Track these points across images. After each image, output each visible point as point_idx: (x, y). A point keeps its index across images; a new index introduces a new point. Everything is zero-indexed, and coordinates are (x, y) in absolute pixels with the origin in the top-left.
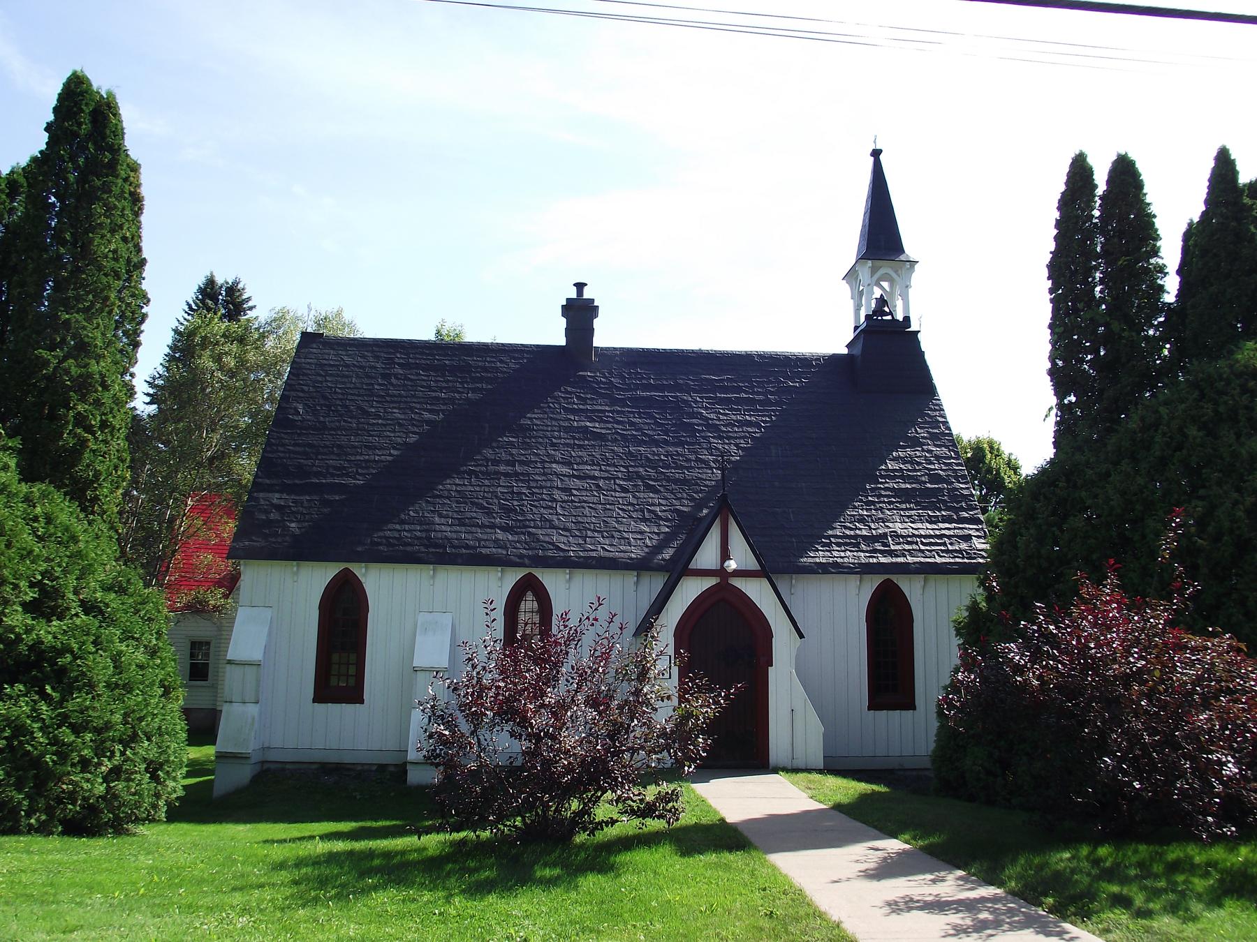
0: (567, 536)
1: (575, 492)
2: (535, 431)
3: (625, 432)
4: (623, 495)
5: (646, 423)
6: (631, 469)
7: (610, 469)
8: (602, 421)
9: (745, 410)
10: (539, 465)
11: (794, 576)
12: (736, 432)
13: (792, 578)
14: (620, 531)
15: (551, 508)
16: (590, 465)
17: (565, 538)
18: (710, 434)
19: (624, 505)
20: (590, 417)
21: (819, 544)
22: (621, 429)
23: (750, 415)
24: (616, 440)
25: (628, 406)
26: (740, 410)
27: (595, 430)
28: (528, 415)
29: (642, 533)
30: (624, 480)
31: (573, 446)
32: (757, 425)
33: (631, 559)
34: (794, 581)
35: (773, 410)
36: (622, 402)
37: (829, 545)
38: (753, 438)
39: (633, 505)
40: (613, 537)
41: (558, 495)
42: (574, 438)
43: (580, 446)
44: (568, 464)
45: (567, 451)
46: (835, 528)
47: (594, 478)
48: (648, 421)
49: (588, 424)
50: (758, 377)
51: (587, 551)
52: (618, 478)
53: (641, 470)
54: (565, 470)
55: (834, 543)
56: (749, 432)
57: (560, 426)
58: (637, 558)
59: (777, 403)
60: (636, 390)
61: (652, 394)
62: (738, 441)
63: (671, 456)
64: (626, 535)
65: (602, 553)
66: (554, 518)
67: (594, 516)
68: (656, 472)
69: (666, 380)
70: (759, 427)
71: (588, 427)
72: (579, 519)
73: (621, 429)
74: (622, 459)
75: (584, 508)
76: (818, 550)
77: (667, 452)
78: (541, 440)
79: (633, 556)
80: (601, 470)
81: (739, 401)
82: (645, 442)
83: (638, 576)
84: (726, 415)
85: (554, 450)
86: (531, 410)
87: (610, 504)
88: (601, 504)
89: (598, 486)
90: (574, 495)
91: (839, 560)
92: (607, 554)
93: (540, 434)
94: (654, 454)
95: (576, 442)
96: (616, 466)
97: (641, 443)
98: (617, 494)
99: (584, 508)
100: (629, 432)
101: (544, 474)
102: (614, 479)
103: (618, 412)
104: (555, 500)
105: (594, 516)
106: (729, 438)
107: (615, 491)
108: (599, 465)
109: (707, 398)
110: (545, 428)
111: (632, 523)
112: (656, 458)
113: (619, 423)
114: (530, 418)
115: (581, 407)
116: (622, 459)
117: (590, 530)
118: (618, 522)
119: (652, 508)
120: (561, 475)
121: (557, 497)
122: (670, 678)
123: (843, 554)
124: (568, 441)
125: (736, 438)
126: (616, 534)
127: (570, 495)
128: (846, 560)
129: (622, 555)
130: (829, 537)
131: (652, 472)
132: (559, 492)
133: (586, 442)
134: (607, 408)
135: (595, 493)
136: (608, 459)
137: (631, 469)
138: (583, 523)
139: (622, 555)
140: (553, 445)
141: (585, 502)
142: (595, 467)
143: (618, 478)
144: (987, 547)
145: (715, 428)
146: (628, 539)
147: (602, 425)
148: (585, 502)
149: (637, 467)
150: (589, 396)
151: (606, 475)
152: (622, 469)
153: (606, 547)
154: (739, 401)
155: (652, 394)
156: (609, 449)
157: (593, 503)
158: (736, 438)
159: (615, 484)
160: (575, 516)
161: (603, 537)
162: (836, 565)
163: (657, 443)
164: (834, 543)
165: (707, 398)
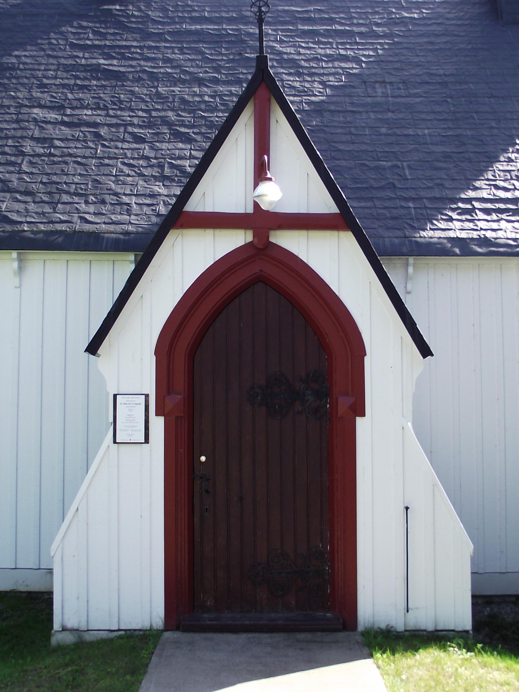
0: (26, 202)
1: (57, 143)
2: (21, 70)
3: (155, 71)
4: (135, 146)
5: (189, 60)
6: (154, 114)
7: (123, 114)
8: (124, 57)
9: (337, 44)
10: (12, 110)
11: (411, 260)
12: (323, 68)
13: (407, 265)
14: (116, 194)
15: (12, 164)
16: (92, 109)
17: (23, 206)
18: (282, 71)
19: (133, 159)
20: (122, 54)
21: (453, 210)
22: (151, 67)
23: (346, 49)
24: (140, 79)
25: (166, 41)
26: (331, 43)
27: (111, 68)
28: (16, 53)
29: (153, 196)
30: (141, 127)
31: (71, 88)
32: (356, 60)
33: (127, 233)
34: (411, 270)
35: (380, 44)
36: (160, 37)
37: (471, 211)
38: (349, 75)
39: (148, 158)
40: (103, 202)
41: (28, 147)
42: (76, 77)
43: (82, 88)
44: (60, 108)
45: (62, 93)
46: (480, 189)
47: (96, 125)
48: (193, 57)
49: (102, 61)
50: (357, 7)
51: (53, 222)
52: (132, 125)
53: (170, 114)
54: (53, 116)
55: (480, 210)
56: (342, 68)
57: (59, 65)
58: (137, 233)
59: (385, 36)
60: (181, 23)
61: (204, 27)
62: (325, 78)
63: (220, 96)
64: (126, 199)
65: (79, 226)
66: (14, 178)
67: (80, 175)
68: (194, 117)
69: (227, 12)
70: (358, 61)
71: (99, 65)
72: (55, 178)
73: (151, 67)
74: (143, 101)
75: (66, 163)
76: (451, 219)
77: (215, 92)
78: (25, 81)
79: (130, 228)
80: (108, 115)
81: (328, 34)
82: (183, 82)
83: (20, 260)
84: (309, 48)
85: (42, 92)
86: (22, 46)
87: (109, 158)
88: (96, 158)
89: (97, 135)
90: (56, 147)
91: (489, 234)
92: (87, 227)
93: (28, 73)
94: (195, 95)
95: (79, 82)
96: (132, 111)
97: (175, 82)
98: (126, 145)
99: (66, 163)
100: (162, 71)
101: (17, 121)
102: (125, 126)
103: (150, 48)
104: (23, 154)
105: (80, 175)
106: (311, 75)
107: (124, 141)
108: (106, 108)
109: (282, 30)
110: (36, 67)
111: (141, 182)
112: (197, 99)
113: (147, 59)
114: (17, 57)
115: (97, 42)
116: (143, 101)
117: (68, 193)
118: (116, 182)
119: (179, 162)
120: (43, 122)
121: (28, 150)
122: (147, 441)
123: (495, 226)
124: (66, 81)
125: (323, 74)
126: (109, 199)
127: (49, 147)
128: (500, 234)
129: (112, 228)
130: (469, 201)
131: (187, 117)
132: (32, 143)
133: (95, 82)
134: (135, 44)
135: (91, 144)
136: (121, 102)
137: (154, 114)
138: (58, 183)
139: (112, 228)
140: (42, 86)
141: (70, 155)
142: (99, 112)
143: (132, 125)
144: (346, 190)
145: (293, 64)
146: (128, 204)
147: (124, 63)
148: (70, 155)
149: (164, 110)
150: (111, 31)
151: (114, 121)
152: (140, 113)
153: (87, 216)
154: (328, 34)
155: (204, 27)
156: (126, 90)
157: (84, 157)
158: (323, 74)
159: (125, 131)
160: (48, 174)
161: (87, 202)
162: (484, 242)
163: (201, 82)
164: (480, 210)
165: (282, 30)
